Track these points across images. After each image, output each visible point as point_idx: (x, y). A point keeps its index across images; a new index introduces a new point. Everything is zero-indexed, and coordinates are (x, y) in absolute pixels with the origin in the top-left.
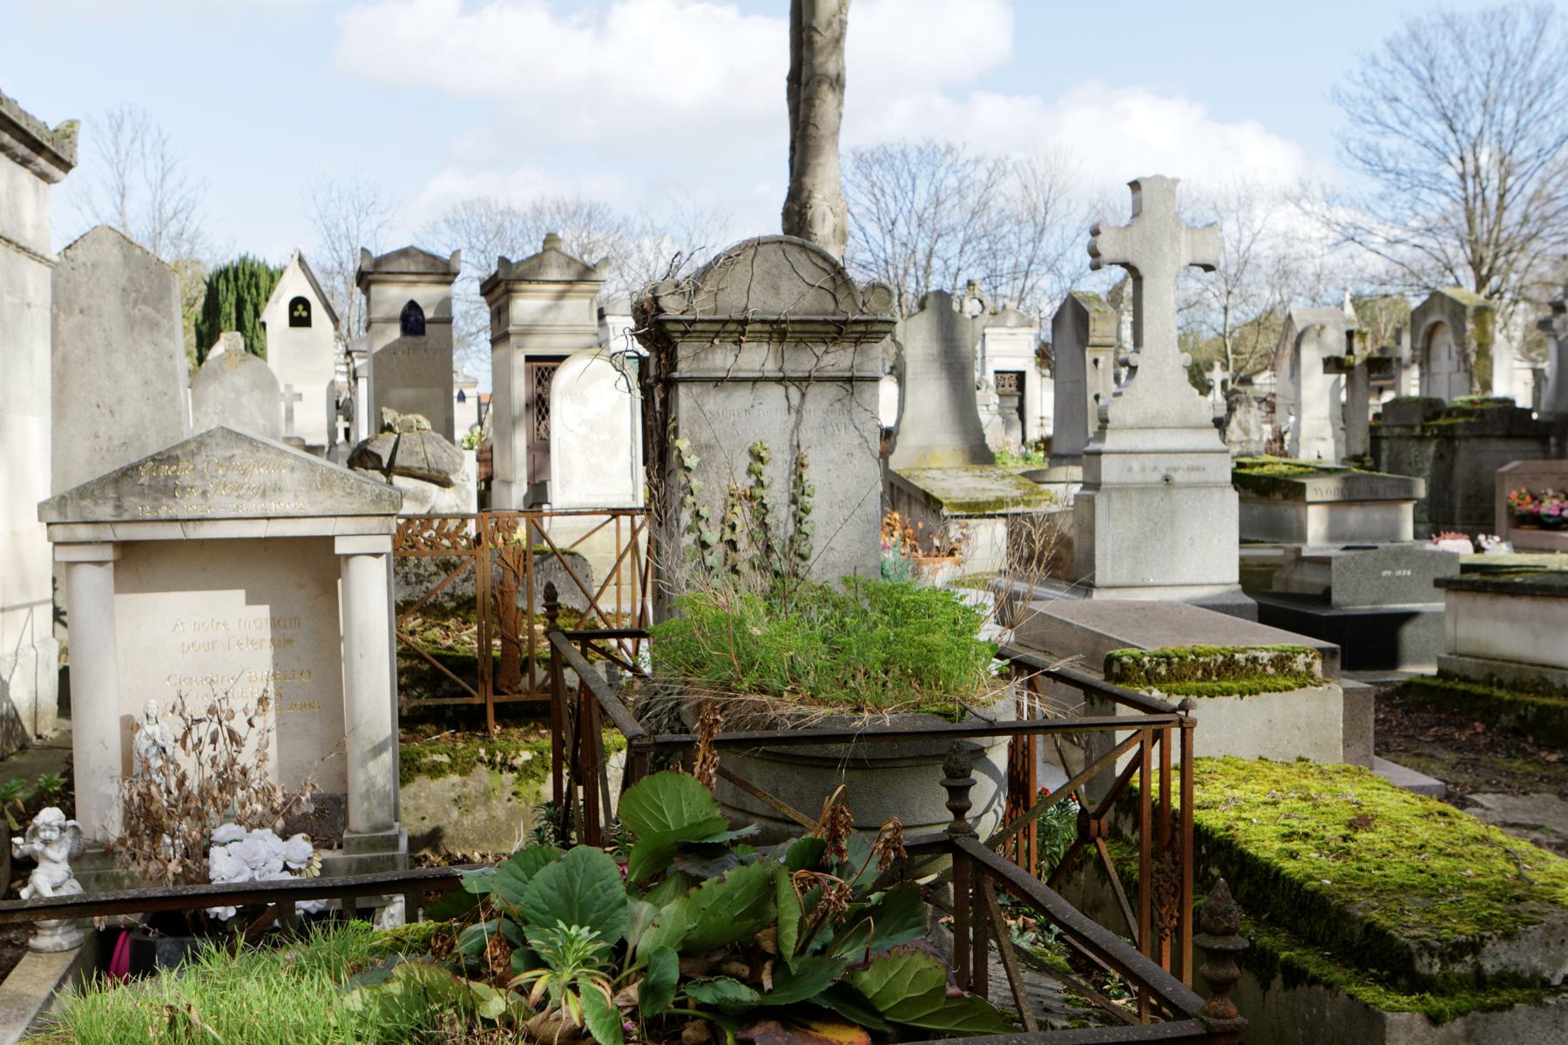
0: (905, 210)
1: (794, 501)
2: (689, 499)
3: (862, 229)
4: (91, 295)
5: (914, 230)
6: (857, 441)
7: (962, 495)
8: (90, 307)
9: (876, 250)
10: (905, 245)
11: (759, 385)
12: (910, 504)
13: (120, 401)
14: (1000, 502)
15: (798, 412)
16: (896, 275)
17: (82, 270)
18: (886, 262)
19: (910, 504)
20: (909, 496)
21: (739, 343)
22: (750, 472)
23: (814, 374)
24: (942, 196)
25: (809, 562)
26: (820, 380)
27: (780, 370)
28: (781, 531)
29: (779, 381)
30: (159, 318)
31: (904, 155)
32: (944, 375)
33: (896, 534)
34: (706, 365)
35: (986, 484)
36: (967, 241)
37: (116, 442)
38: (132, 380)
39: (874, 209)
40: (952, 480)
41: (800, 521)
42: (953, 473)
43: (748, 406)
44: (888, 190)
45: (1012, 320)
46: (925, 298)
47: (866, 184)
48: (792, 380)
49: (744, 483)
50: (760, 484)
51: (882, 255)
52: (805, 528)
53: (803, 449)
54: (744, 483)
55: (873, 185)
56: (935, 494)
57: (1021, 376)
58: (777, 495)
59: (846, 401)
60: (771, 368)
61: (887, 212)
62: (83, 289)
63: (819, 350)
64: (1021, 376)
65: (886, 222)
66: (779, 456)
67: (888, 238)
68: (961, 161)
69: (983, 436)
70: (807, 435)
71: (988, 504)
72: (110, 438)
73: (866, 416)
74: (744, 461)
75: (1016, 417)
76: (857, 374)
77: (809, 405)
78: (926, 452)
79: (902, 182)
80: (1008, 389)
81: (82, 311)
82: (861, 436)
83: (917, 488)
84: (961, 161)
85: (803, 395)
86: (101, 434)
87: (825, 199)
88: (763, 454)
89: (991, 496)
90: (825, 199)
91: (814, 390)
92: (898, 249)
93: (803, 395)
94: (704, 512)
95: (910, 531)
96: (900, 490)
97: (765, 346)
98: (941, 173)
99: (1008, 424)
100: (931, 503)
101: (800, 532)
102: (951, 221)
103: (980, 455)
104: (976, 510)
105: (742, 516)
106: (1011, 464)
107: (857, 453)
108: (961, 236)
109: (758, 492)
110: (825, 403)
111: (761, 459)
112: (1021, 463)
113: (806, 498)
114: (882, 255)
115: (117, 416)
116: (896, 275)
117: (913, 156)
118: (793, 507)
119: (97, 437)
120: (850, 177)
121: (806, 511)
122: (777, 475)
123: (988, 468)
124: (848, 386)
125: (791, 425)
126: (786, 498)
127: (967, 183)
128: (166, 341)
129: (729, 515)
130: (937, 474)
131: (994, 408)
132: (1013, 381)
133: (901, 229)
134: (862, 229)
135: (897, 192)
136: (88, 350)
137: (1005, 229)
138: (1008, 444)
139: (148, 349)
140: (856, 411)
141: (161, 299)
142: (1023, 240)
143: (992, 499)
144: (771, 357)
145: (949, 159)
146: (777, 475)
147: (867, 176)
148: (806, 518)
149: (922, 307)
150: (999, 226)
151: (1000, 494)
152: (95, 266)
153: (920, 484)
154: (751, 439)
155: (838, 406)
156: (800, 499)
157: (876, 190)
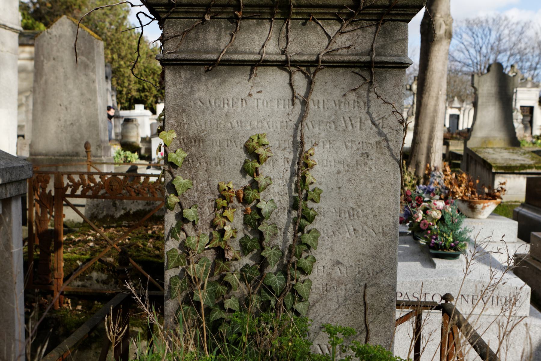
0: (486, 43)
1: (294, 206)
2: (173, 199)
3: (468, 50)
4: (58, 51)
5: (489, 51)
6: (375, 139)
7: (503, 162)
8: (58, 57)
9: (473, 58)
10: (485, 56)
11: (259, 70)
12: (476, 164)
13: (70, 103)
14: (523, 167)
15: (304, 103)
16: (481, 69)
17: (55, 39)
18: (477, 63)
19: (476, 164)
20: (476, 161)
21: (234, 20)
22: (245, 171)
23: (322, 58)
24: (502, 37)
25: (310, 277)
26: (331, 65)
27: (283, 52)
28: (279, 241)
29: (282, 65)
30: (88, 62)
31: (487, 21)
32: (497, 103)
33: (463, 185)
34: (198, 46)
35: (515, 157)
36: (511, 55)
37: (68, 123)
38: (76, 93)
39: (473, 43)
40: (498, 154)
41: (301, 229)
42: (499, 150)
43: (245, 95)
44: (479, 35)
45: (529, 85)
46: (490, 66)
47: (470, 33)
48: (296, 64)
49: (237, 182)
50: (255, 185)
51: (475, 61)
52: (308, 238)
53: (307, 147)
54: (237, 182)
55: (473, 33)
56: (489, 161)
57: (531, 109)
58: (275, 196)
59: (363, 92)
60: (272, 50)
61: (478, 44)
62: (55, 48)
63: (332, 29)
64: (531, 109)
65: (478, 48)
66: (280, 154)
67: (478, 54)
68: (511, 23)
69: (515, 133)
70: (312, 131)
71: (516, 167)
72: (65, 121)
73: (386, 110)
74: (238, 157)
75: (529, 125)
76: (376, 58)
77: (317, 95)
78: (486, 141)
79: (485, 32)
80: (525, 113)
81: (54, 59)
82: (380, 134)
83: (480, 157)
84: (511, 23)
85: (310, 83)
86: (61, 119)
87: (441, 17)
88: (260, 151)
89: (518, 163)
90: (441, 17)
91: (323, 78)
92: (482, 58)
93: (310, 83)
94: (190, 213)
95: (472, 183)
96: (472, 158)
97: (267, 25)
98: (502, 28)
99: (526, 128)
100: (486, 165)
101: (300, 243)
102: (505, 47)
103: (514, 142)
104: (510, 170)
105: (235, 223)
106: (526, 145)
107: (373, 154)
108: (508, 53)
109: (252, 194)
110: (338, 93)
111: (257, 157)
112: (531, 145)
113: (310, 204)
114: (475, 61)
115: (69, 110)
116: (481, 69)
117: (490, 22)
118: (294, 213)
119: (60, 120)
120: (464, 30)
121: (310, 219)
122: (276, 174)
123: (517, 148)
124: (366, 74)
125: (295, 118)
126: (286, 202)
127: (512, 32)
128: (91, 74)
129: (220, 221)
130: (491, 151)
131: (520, 121)
132: (528, 110)
133: (484, 50)
134: (468, 50)
135: (483, 36)
136: (57, 78)
137: (527, 51)
138: (525, 137)
139: (83, 78)
140: (375, 103)
141: (89, 53)
142: (535, 55)
143: (518, 165)
144: (273, 37)
145: (505, 23)
146: (276, 174)
147: (471, 30)
148: (309, 227)
149: (488, 70)
150: (525, 49)
151: (523, 162)
152: (60, 36)
153: (482, 156)
154: (247, 132)
155: (352, 96)
156: (301, 204)
157: (475, 36)
